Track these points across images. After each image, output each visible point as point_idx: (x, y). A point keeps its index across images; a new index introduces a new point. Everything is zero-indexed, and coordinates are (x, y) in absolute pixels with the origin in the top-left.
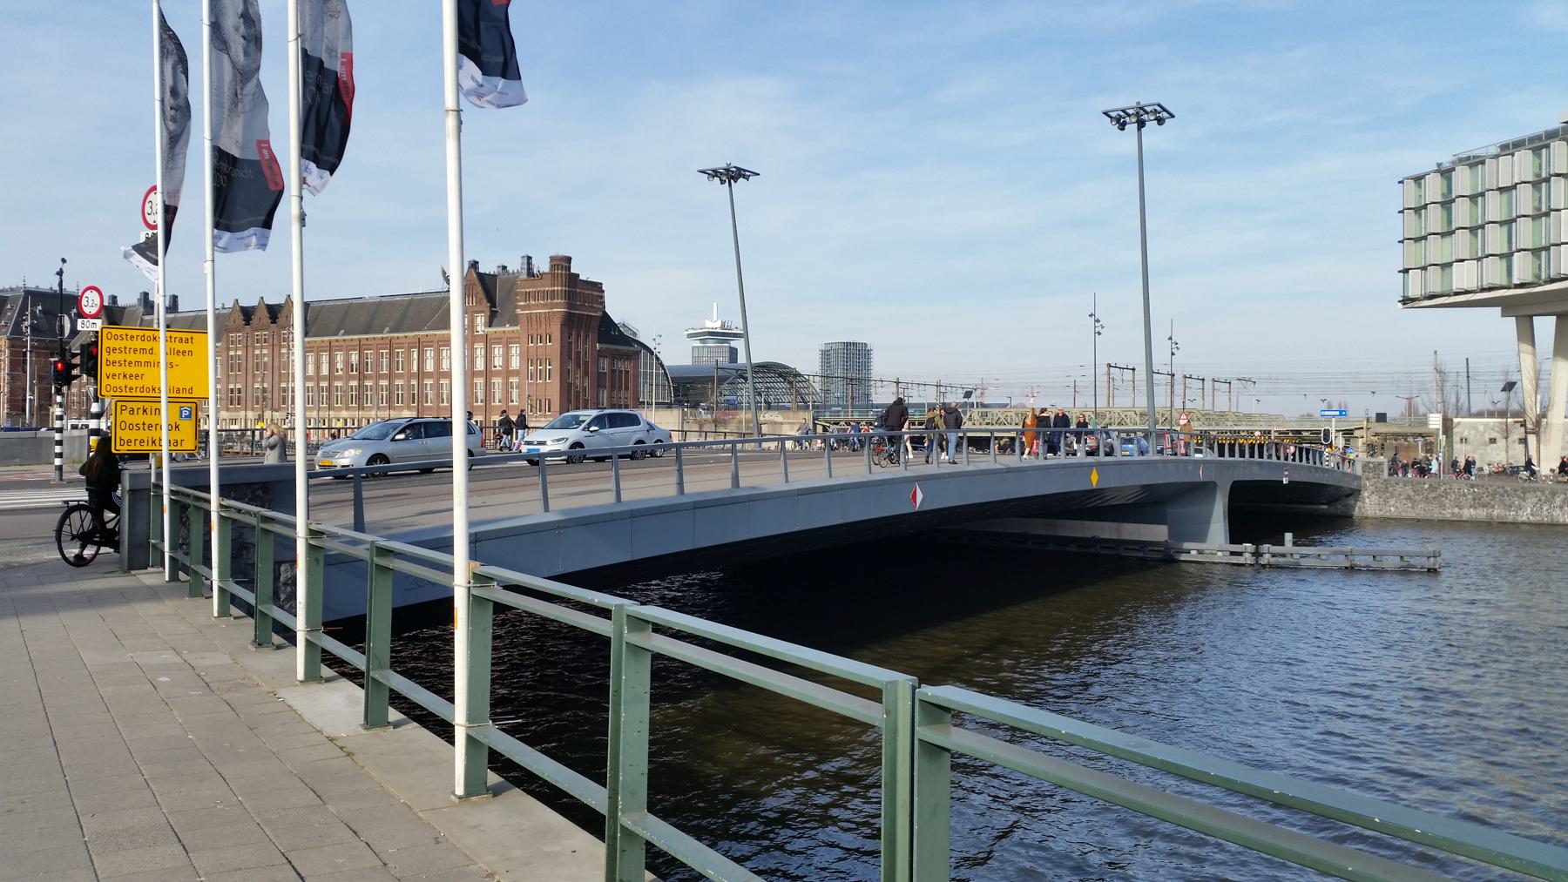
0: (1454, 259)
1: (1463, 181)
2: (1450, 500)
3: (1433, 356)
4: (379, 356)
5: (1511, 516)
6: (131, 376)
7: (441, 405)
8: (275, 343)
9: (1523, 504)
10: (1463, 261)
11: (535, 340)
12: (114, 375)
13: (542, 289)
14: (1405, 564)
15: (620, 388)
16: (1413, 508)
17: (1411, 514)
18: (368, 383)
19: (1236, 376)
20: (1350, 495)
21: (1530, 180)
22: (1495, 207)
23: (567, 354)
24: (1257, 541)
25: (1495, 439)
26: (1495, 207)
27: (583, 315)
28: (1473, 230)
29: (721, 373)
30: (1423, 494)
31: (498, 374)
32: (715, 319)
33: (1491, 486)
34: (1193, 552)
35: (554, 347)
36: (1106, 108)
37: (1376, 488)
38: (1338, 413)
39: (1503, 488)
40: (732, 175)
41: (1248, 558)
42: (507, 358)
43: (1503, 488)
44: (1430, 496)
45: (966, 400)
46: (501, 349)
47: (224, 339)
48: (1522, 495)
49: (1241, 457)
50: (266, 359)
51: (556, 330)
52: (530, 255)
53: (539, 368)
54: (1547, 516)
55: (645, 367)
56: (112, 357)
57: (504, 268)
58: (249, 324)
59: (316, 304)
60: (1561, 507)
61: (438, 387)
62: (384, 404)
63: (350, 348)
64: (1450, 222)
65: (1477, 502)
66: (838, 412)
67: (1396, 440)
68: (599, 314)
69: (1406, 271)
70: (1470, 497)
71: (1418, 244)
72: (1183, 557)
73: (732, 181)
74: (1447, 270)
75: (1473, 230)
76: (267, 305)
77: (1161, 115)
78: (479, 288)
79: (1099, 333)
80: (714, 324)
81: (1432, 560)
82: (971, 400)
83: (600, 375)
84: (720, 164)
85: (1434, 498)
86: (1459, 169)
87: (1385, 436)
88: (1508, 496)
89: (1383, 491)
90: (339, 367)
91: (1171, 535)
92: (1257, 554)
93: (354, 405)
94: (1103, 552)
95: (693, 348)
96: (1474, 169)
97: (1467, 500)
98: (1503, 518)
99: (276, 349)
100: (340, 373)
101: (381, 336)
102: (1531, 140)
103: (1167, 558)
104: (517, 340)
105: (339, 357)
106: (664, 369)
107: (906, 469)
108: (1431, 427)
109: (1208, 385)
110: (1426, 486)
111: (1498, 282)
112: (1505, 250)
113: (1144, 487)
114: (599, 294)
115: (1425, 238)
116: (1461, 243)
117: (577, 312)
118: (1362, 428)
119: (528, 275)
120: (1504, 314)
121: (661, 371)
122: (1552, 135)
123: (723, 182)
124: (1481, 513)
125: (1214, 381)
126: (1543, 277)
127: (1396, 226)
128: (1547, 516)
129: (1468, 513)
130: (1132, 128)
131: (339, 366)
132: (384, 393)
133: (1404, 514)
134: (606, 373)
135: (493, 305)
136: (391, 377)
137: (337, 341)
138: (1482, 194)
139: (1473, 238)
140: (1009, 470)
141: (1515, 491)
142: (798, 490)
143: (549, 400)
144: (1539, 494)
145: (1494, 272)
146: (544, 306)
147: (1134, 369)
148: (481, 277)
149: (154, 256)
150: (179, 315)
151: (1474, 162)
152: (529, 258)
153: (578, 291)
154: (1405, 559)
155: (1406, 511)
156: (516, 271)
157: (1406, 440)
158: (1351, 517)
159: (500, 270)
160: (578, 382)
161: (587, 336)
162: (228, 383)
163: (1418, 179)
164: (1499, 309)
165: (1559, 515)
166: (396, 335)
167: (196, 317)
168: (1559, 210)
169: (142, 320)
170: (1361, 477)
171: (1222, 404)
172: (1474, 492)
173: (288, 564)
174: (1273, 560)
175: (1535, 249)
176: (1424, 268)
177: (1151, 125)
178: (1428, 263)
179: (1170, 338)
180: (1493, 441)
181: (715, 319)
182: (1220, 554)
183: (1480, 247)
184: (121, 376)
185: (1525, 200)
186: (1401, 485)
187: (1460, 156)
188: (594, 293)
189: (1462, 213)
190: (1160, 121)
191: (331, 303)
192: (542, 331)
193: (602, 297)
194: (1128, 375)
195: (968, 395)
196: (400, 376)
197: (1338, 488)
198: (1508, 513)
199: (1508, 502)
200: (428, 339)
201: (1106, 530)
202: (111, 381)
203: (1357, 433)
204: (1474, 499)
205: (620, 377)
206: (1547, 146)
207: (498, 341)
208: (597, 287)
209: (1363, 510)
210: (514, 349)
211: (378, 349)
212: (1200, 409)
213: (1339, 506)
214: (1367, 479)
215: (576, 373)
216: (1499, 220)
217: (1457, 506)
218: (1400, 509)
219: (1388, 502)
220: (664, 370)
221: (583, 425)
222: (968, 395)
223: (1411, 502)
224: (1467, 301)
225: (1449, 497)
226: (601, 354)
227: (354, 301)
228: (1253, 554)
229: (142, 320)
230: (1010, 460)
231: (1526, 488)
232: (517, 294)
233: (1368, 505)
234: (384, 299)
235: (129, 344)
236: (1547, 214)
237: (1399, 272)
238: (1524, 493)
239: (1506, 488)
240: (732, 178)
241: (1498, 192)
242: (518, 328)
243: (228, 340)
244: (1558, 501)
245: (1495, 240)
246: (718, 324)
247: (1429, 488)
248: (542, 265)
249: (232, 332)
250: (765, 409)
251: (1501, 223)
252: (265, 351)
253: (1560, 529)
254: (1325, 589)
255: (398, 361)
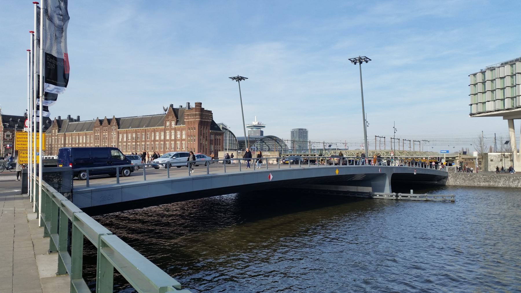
0: (486, 101)
1: (489, 75)
2: (477, 180)
3: (482, 133)
4: (151, 134)
5: (496, 185)
6: (23, 144)
7: (161, 150)
8: (110, 131)
9: (500, 181)
10: (489, 101)
11: (190, 129)
12: (19, 144)
13: (193, 113)
14: (444, 199)
15: (218, 144)
16: (465, 182)
17: (464, 184)
18: (138, 143)
19: (422, 140)
20: (444, 178)
21: (510, 75)
22: (499, 84)
23: (200, 134)
24: (397, 192)
25: (492, 160)
26: (499, 84)
27: (205, 121)
28: (492, 91)
29: (250, 139)
30: (468, 178)
31: (179, 140)
32: (256, 121)
33: (490, 175)
34: (378, 196)
35: (196, 132)
36: (349, 58)
37: (453, 176)
38: (446, 152)
39: (494, 175)
40: (239, 79)
41: (394, 198)
42: (181, 135)
43: (494, 175)
44: (470, 178)
45: (329, 148)
46: (185, 132)
47: (94, 130)
48: (500, 178)
49: (422, 167)
50: (107, 136)
51: (197, 126)
52: (189, 102)
53: (191, 138)
54: (508, 185)
55: (225, 137)
56: (19, 140)
57: (181, 106)
58: (101, 125)
59: (123, 119)
60: (512, 182)
61: (171, 144)
62: (125, 151)
63: (132, 133)
64: (485, 89)
65: (485, 181)
66: (291, 152)
67: (469, 160)
68: (211, 121)
69: (471, 105)
70: (483, 179)
71: (475, 96)
72: (375, 197)
73: (240, 81)
74: (484, 104)
75: (492, 91)
76: (107, 119)
77: (367, 60)
78: (173, 113)
79: (368, 126)
80: (255, 123)
81: (453, 198)
82: (331, 148)
83: (211, 140)
84: (236, 76)
85: (471, 179)
86: (487, 71)
87: (466, 159)
88: (495, 178)
89: (455, 177)
90: (129, 139)
91: (373, 190)
92: (397, 196)
93: (134, 150)
94: (351, 196)
95: (249, 131)
96: (492, 71)
97: (482, 180)
98: (493, 185)
99: (110, 133)
100: (130, 140)
101: (142, 128)
102: (510, 62)
103: (370, 197)
104: (185, 129)
105: (130, 135)
106: (235, 138)
107: (267, 169)
108: (474, 156)
109: (412, 142)
110: (469, 175)
111: (500, 108)
112: (503, 98)
113: (366, 174)
114: (211, 114)
115: (477, 94)
116: (488, 96)
117: (203, 120)
118: (458, 157)
119: (188, 108)
120: (504, 119)
121: (235, 139)
122: (517, 60)
123: (237, 81)
124: (486, 184)
125: (414, 141)
126: (515, 106)
127: (470, 90)
128: (508, 185)
129: (482, 184)
130: (358, 64)
131: (130, 138)
132: (143, 147)
133: (462, 184)
134: (213, 140)
135: (177, 118)
136: (145, 141)
137: (129, 130)
138: (495, 80)
139: (492, 94)
140: (304, 169)
141: (497, 177)
142: (228, 175)
143: (195, 149)
144: (505, 178)
145: (499, 105)
146: (193, 119)
147: (385, 138)
148: (174, 109)
149: (47, 109)
150: (80, 122)
151: (492, 69)
152: (189, 103)
153: (204, 113)
154: (444, 198)
155: (463, 183)
156: (185, 107)
157: (472, 160)
158: (445, 185)
159: (180, 107)
160: (204, 142)
161: (207, 128)
162: (95, 144)
163: (475, 75)
164: (502, 117)
165: (512, 184)
166: (147, 128)
167: (85, 123)
168: (519, 85)
169: (68, 124)
170: (448, 172)
171: (417, 149)
172: (484, 177)
173: (66, 193)
174: (402, 198)
175: (512, 97)
176: (477, 104)
177: (364, 63)
178: (478, 102)
179: (394, 127)
180: (492, 160)
181: (256, 121)
182: (386, 196)
183: (494, 97)
184: (21, 144)
185: (508, 81)
186: (461, 175)
187: (489, 67)
188: (209, 114)
189: (489, 86)
190: (367, 62)
191: (127, 118)
192: (192, 126)
193: (212, 115)
194: (383, 139)
195: (330, 146)
196: (148, 141)
197: (440, 176)
198: (495, 184)
199: (495, 180)
200: (157, 129)
201: (353, 189)
202: (18, 146)
203: (456, 158)
204: (484, 179)
205: (218, 141)
206: (515, 64)
207: (179, 130)
208: (210, 112)
209: (449, 183)
210: (184, 132)
211: (141, 133)
212: (398, 150)
213: (441, 182)
214: (450, 173)
215: (203, 140)
216: (500, 88)
217: (479, 182)
218: (461, 183)
219: (457, 180)
220: (236, 138)
221: (171, 157)
222: (330, 146)
223: (464, 181)
224: (491, 115)
225: (476, 179)
226: (211, 134)
227: (134, 117)
228: (396, 196)
229: (68, 124)
230: (313, 166)
231: (501, 176)
232: (185, 115)
233: (450, 181)
234: (144, 117)
235: (23, 136)
236: (515, 86)
237: (469, 105)
238: (500, 177)
239: (495, 176)
240: (240, 79)
241: (500, 79)
242: (185, 125)
243: (95, 130)
244: (511, 180)
245: (499, 94)
246: (257, 123)
247: (470, 176)
248: (193, 105)
249: (96, 128)
250: (267, 151)
251: (501, 89)
252: (106, 134)
253: (458, 187)
254: (437, 207)
255: (148, 136)
